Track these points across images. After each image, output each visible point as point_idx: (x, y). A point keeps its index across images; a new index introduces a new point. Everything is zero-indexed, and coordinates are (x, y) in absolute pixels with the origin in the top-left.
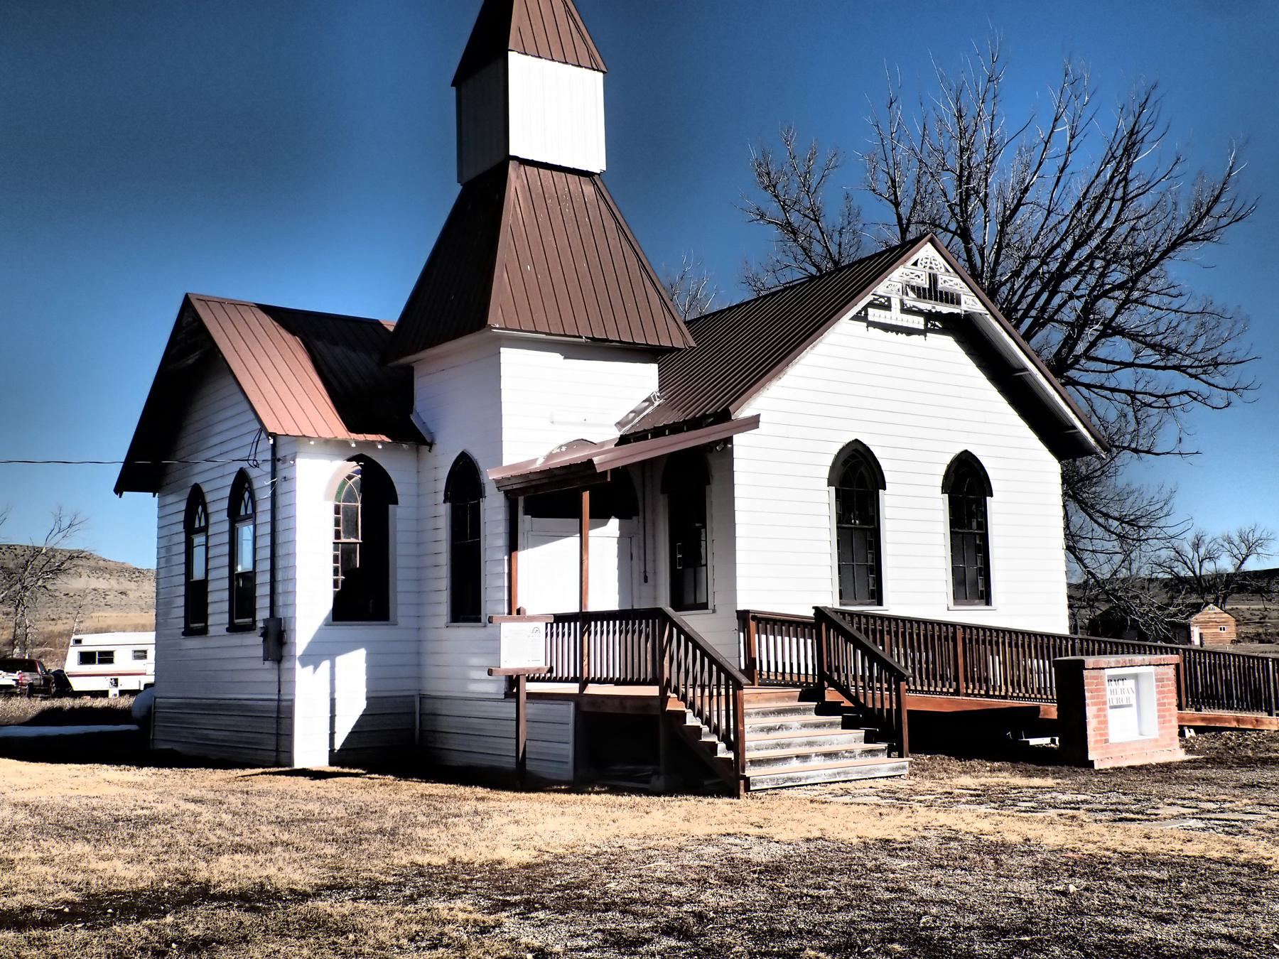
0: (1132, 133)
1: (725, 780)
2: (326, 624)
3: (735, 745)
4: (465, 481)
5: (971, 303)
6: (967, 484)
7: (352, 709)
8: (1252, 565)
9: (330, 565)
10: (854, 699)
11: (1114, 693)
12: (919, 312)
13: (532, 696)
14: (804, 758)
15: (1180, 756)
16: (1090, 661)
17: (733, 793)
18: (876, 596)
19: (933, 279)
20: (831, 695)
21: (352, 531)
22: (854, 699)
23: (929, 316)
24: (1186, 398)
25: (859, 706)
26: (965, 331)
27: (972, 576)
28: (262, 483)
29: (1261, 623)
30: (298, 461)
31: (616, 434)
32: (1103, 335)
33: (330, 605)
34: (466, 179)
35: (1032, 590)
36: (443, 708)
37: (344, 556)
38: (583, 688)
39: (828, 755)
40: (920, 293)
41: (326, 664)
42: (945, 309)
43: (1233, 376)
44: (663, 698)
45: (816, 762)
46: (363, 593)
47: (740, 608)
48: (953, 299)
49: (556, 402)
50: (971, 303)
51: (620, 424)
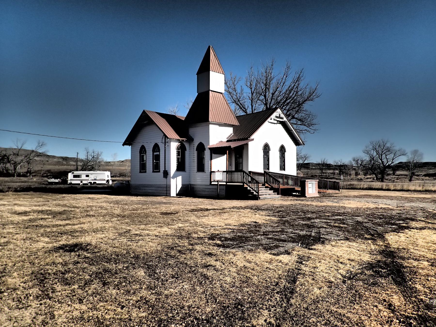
0: (298, 78)
1: (256, 198)
2: (175, 171)
3: (258, 193)
4: (201, 148)
5: (285, 119)
6: (282, 150)
7: (180, 186)
8: (306, 162)
10: (271, 186)
11: (310, 185)
12: (276, 120)
13: (220, 185)
14: (266, 195)
15: (318, 196)
16: (307, 180)
17: (258, 200)
18: (268, 169)
19: (280, 115)
20: (267, 185)
21: (179, 155)
22: (271, 186)
23: (278, 121)
24: (306, 131)
25: (272, 187)
26: (284, 124)
27: (283, 167)
28: (161, 146)
29: (307, 175)
30: (171, 143)
31: (226, 140)
32: (292, 119)
33: (176, 168)
34: (200, 92)
35: (291, 169)
36: (195, 187)
37: (178, 159)
39: (269, 194)
40: (277, 117)
42: (281, 120)
43: (315, 127)
44: (244, 185)
45: (268, 195)
46: (181, 167)
47: (249, 170)
48: (282, 118)
50: (285, 119)
51: (227, 138)
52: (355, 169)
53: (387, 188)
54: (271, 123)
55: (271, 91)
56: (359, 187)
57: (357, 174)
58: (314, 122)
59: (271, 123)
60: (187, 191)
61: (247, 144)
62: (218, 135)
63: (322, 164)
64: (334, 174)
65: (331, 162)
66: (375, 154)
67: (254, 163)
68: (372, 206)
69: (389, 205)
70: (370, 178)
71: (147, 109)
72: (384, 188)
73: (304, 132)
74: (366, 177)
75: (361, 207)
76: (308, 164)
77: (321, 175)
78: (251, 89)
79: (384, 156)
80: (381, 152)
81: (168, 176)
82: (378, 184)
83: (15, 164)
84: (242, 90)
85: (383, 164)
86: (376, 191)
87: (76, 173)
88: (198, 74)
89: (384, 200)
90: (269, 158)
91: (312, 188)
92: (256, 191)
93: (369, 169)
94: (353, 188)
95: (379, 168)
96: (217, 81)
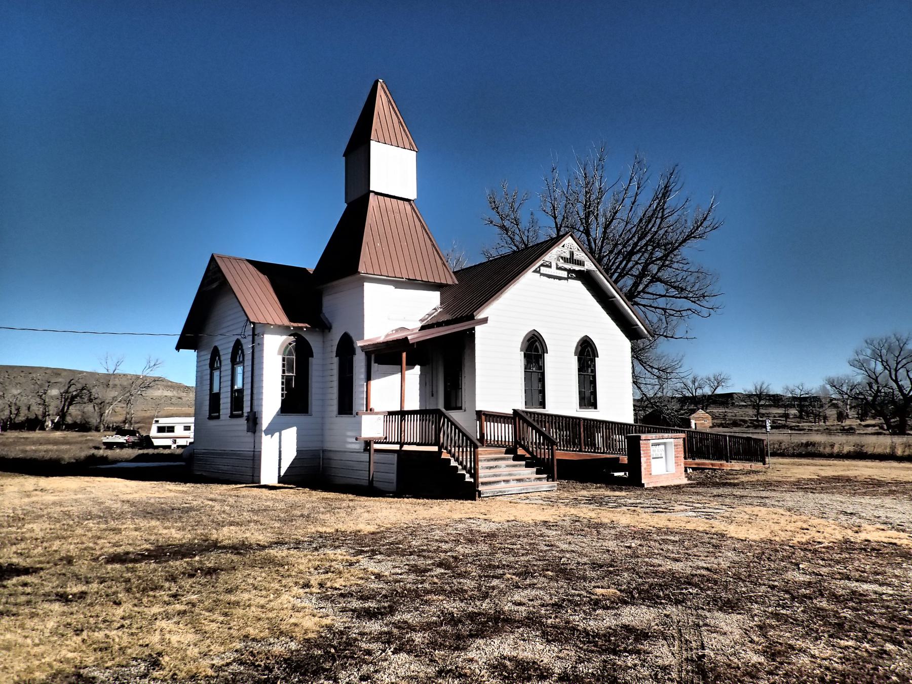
2: (278, 414)
3: (474, 475)
4: (346, 347)
5: (589, 266)
6: (586, 352)
7: (290, 455)
8: (719, 391)
9: (280, 386)
12: (565, 269)
13: (377, 451)
14: (507, 481)
18: (543, 404)
19: (572, 254)
20: (520, 452)
25: (534, 457)
26: (586, 278)
27: (588, 398)
29: (724, 419)
30: (265, 336)
31: (420, 325)
32: (651, 281)
33: (279, 406)
34: (352, 199)
36: (332, 455)
38: (401, 447)
41: (277, 434)
42: (577, 268)
44: (440, 452)
45: (513, 483)
46: (295, 401)
48: (580, 263)
49: (391, 310)
50: (589, 266)
52: (835, 406)
53: (906, 453)
54: (549, 276)
55: (602, 220)
56: (828, 450)
57: (841, 417)
58: (708, 291)
59: (549, 276)
60: (313, 472)
61: (470, 336)
62: (391, 310)
63: (756, 395)
64: (786, 416)
65: (776, 389)
66: (880, 368)
67: (496, 384)
68: (831, 532)
69: (900, 528)
70: (874, 426)
71: (217, 252)
72: (899, 452)
73: (684, 313)
74: (863, 423)
75: (784, 536)
76: (730, 395)
77: (757, 421)
78: (555, 218)
79: (902, 372)
80: (893, 364)
81: (258, 426)
82: (883, 443)
83: (102, 405)
84: (533, 222)
85: (903, 394)
86: (877, 463)
87: (164, 422)
88: (346, 155)
89: (888, 501)
90: (543, 374)
91: (663, 460)
92: (469, 472)
93: (872, 404)
94: (809, 452)
95: (893, 402)
96: (393, 168)
